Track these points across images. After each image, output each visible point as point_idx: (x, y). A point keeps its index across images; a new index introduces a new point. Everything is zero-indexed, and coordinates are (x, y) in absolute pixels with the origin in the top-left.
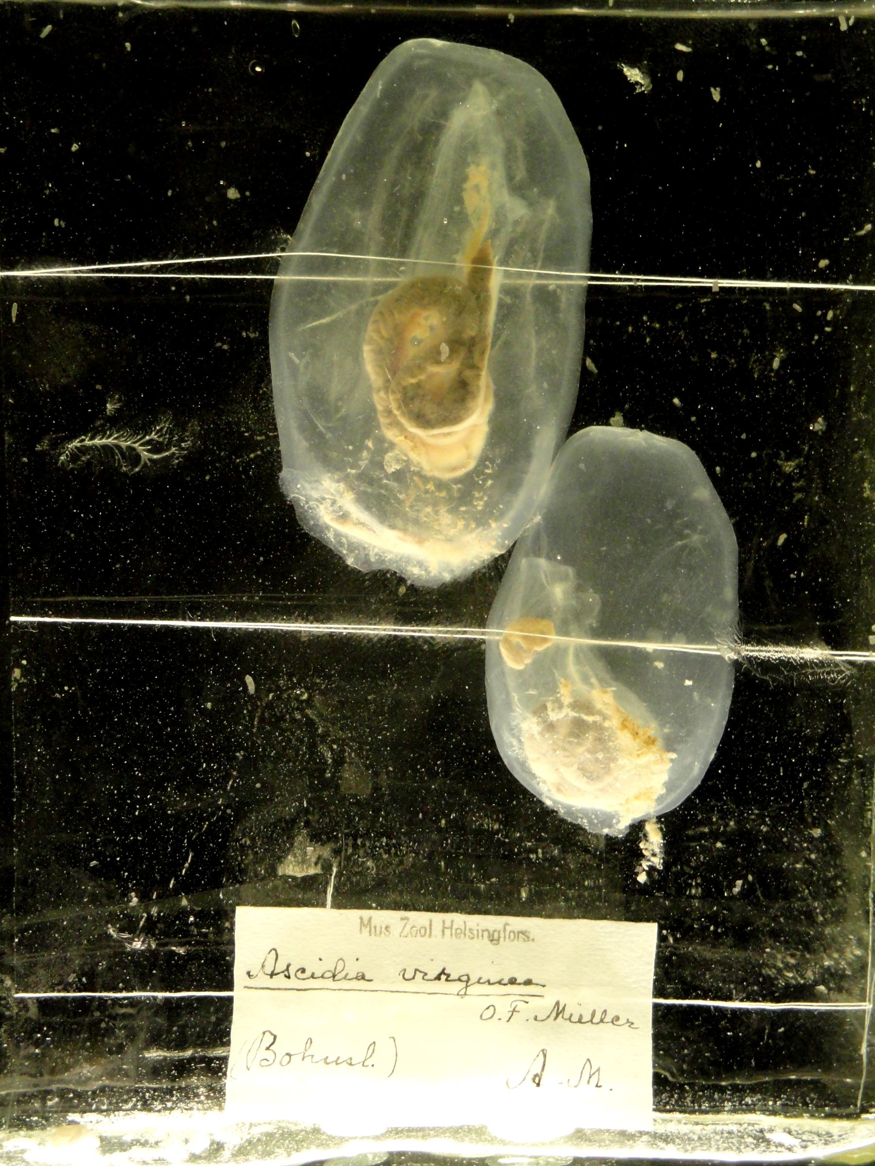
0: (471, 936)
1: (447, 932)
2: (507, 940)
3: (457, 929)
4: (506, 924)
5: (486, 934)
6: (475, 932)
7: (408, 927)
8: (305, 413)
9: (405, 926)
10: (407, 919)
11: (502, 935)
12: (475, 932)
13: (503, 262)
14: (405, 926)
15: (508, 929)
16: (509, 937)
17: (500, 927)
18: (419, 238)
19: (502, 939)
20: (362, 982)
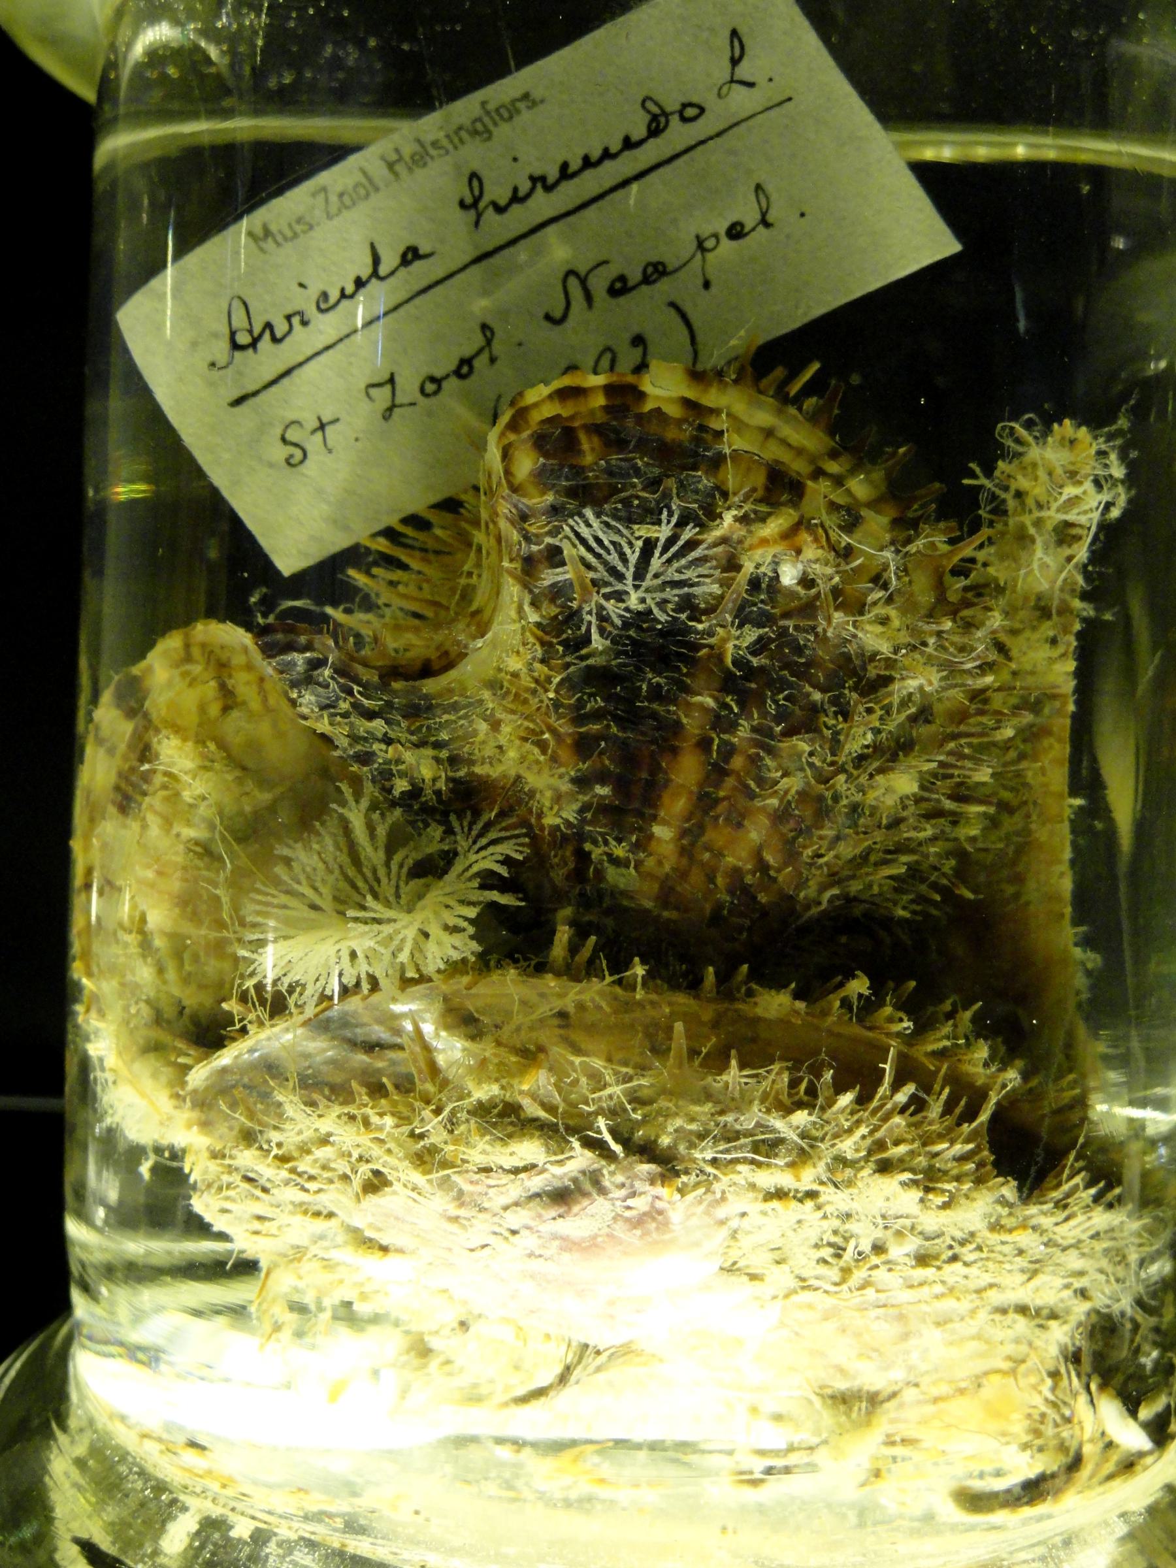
0: (442, 152)
1: (398, 168)
2: (500, 122)
3: (341, 195)
4: (484, 104)
5: (463, 134)
6: (445, 142)
7: (334, 199)
8: (686, 910)
9: (327, 200)
10: (324, 189)
11: (486, 120)
12: (445, 142)
13: (469, 1095)
14: (327, 200)
15: (491, 107)
16: (501, 117)
17: (477, 111)
18: (192, 1052)
19: (491, 127)
20: (417, 265)
